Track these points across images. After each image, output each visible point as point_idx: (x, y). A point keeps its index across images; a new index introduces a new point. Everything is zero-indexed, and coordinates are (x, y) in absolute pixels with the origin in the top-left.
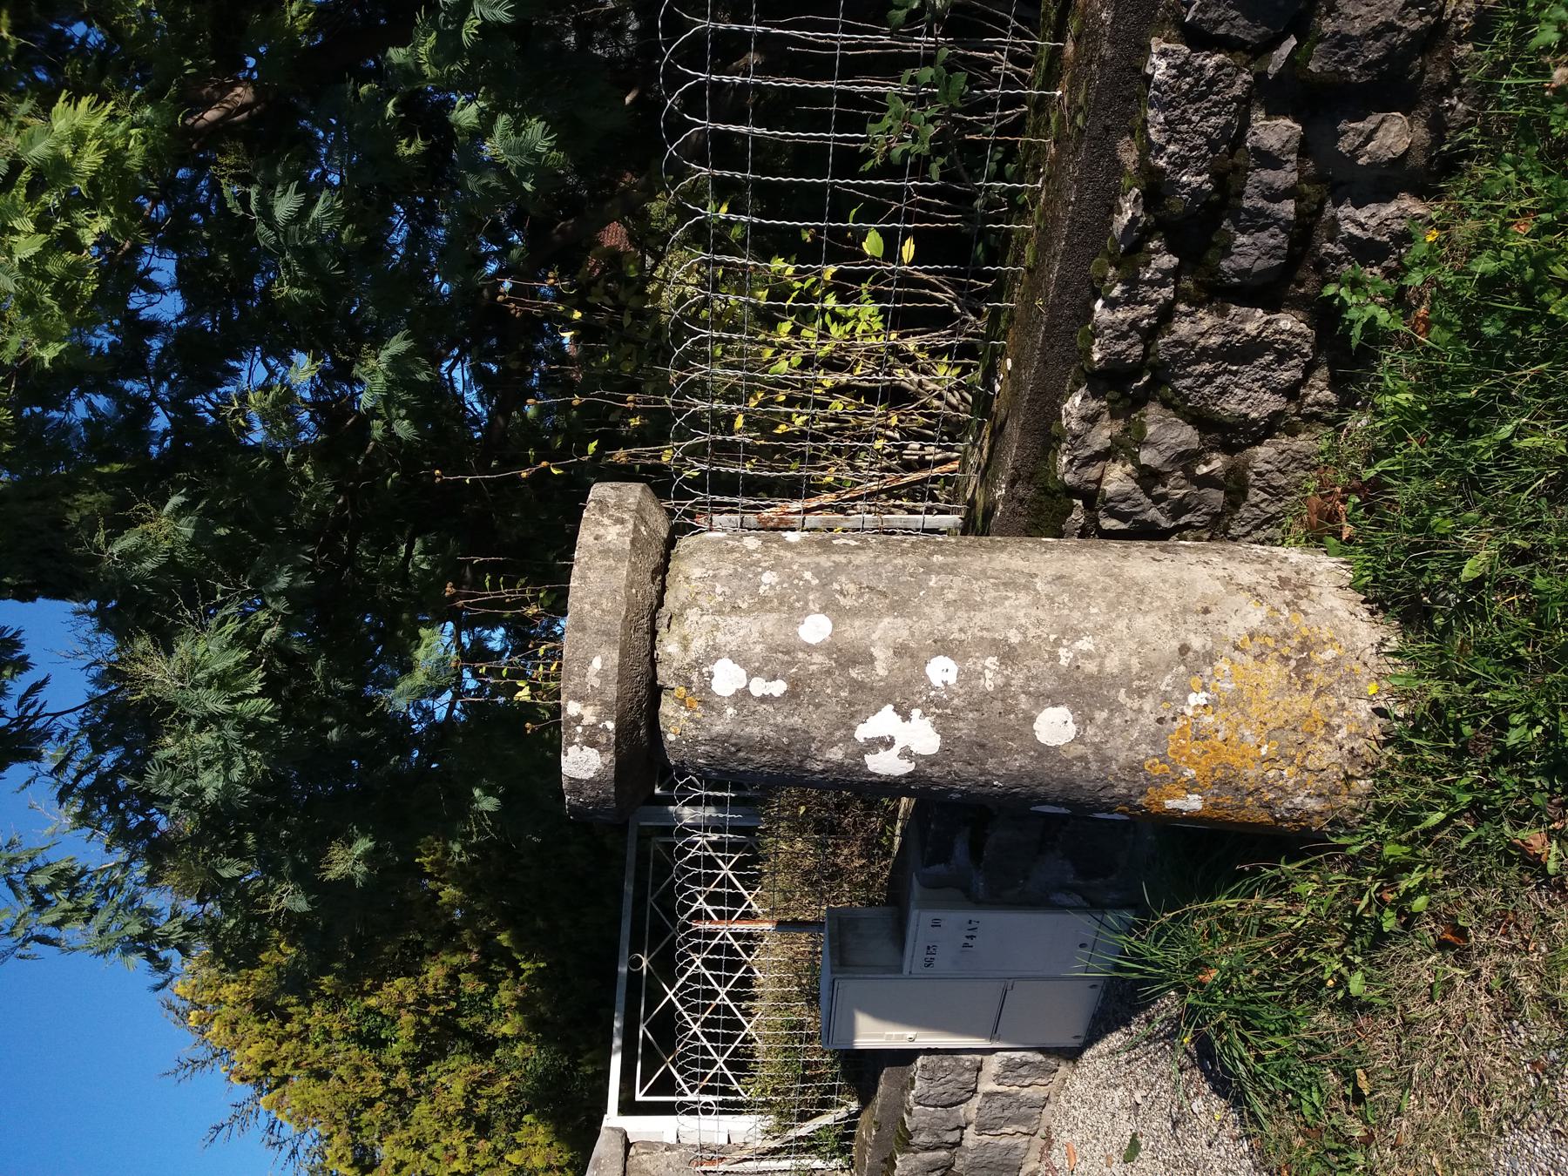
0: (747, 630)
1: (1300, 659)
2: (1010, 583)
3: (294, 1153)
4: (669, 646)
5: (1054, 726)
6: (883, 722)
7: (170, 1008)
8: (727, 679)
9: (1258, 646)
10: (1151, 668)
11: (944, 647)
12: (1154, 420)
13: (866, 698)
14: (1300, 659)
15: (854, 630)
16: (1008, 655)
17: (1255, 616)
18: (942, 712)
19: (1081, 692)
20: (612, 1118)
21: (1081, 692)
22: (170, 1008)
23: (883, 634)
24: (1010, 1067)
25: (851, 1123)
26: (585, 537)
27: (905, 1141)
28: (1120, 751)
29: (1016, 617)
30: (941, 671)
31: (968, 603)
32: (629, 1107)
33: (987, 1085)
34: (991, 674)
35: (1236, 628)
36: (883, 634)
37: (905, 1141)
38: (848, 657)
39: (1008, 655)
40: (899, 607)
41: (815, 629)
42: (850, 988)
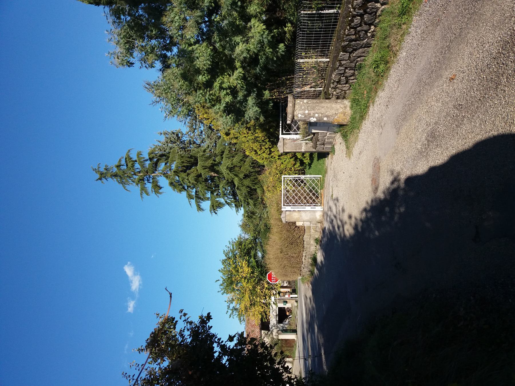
0: (301, 112)
1: (344, 114)
2: (323, 107)
3: (185, 123)
4: (295, 113)
5: (325, 119)
6: (312, 118)
7: (146, 88)
8: (300, 116)
9: (341, 113)
10: (333, 115)
11: (317, 113)
12: (337, 90)
13: (311, 117)
14: (344, 114)
15: (310, 112)
16: (322, 114)
17: (342, 110)
18: (317, 118)
19: (327, 116)
20: (281, 136)
21: (327, 116)
22: (146, 88)
23: (312, 112)
24: (330, 134)
25: (312, 137)
26: (288, 105)
27: (318, 140)
28: (330, 120)
29: (323, 111)
30: (317, 115)
31: (319, 109)
32: (283, 134)
33: (328, 135)
34: (320, 115)
35: (340, 111)
36: (312, 112)
37: (318, 140)
38: (309, 114)
39: (322, 114)
40: (313, 110)
41: (307, 112)
42: (311, 127)
